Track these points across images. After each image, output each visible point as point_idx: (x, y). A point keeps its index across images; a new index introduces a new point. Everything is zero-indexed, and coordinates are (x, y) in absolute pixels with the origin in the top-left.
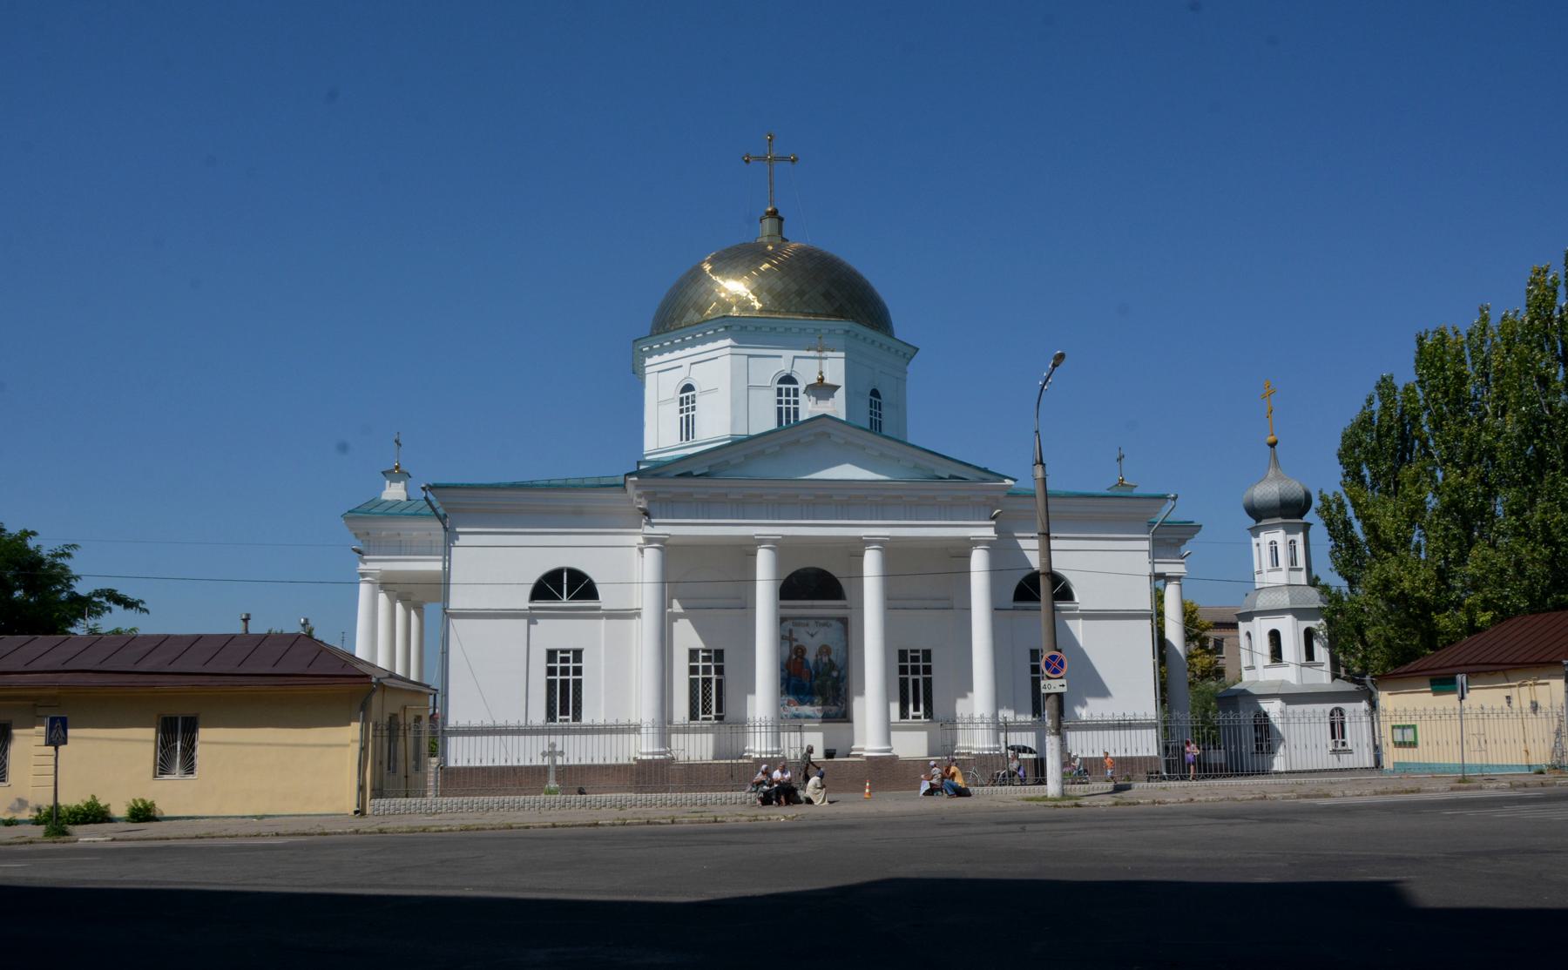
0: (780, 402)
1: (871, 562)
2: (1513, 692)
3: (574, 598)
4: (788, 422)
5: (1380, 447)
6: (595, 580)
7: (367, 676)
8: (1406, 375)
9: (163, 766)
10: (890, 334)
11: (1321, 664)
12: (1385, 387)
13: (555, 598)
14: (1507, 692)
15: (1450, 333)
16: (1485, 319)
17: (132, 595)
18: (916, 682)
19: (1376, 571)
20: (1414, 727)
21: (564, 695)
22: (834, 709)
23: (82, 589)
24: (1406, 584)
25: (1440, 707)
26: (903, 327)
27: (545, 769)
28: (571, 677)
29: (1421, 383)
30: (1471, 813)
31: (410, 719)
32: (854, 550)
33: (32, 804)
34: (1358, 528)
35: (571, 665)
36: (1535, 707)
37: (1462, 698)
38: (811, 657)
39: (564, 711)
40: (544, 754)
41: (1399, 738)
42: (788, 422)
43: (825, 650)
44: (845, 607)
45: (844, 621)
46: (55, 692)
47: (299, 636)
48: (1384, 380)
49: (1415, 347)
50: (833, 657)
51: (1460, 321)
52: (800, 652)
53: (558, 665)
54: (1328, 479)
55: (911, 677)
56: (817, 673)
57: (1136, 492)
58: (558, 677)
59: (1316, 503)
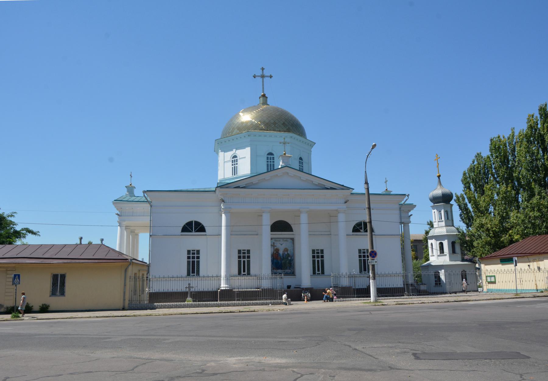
0: (268, 162)
1: (304, 218)
2: (531, 264)
3: (197, 231)
4: (271, 169)
5: (477, 178)
6: (204, 225)
7: (127, 259)
8: (486, 153)
9: (53, 293)
10: (306, 138)
11: (446, 255)
12: (478, 156)
13: (191, 232)
14: (529, 264)
15: (501, 137)
16: (513, 133)
17: (35, 230)
18: (318, 261)
19: (478, 221)
20: (495, 276)
21: (193, 267)
22: (289, 271)
23: (18, 228)
24: (489, 226)
25: (503, 269)
26: (310, 136)
27: (187, 293)
28: (196, 260)
29: (492, 155)
30: (527, 306)
31: (141, 275)
32: (297, 214)
33: (5, 306)
34: (469, 206)
35: (196, 255)
36: (539, 268)
37: (516, 265)
38: (281, 252)
39: (193, 272)
40: (186, 288)
41: (489, 280)
42: (271, 169)
43: (286, 250)
44: (293, 235)
45: (293, 239)
46: (14, 265)
47: (77, 245)
48: (478, 154)
49: (490, 143)
50: (289, 252)
51: (505, 134)
52: (277, 250)
53: (191, 255)
54: (458, 189)
55: (242, 260)
56: (283, 258)
57: (392, 193)
58: (191, 260)
59: (454, 198)
